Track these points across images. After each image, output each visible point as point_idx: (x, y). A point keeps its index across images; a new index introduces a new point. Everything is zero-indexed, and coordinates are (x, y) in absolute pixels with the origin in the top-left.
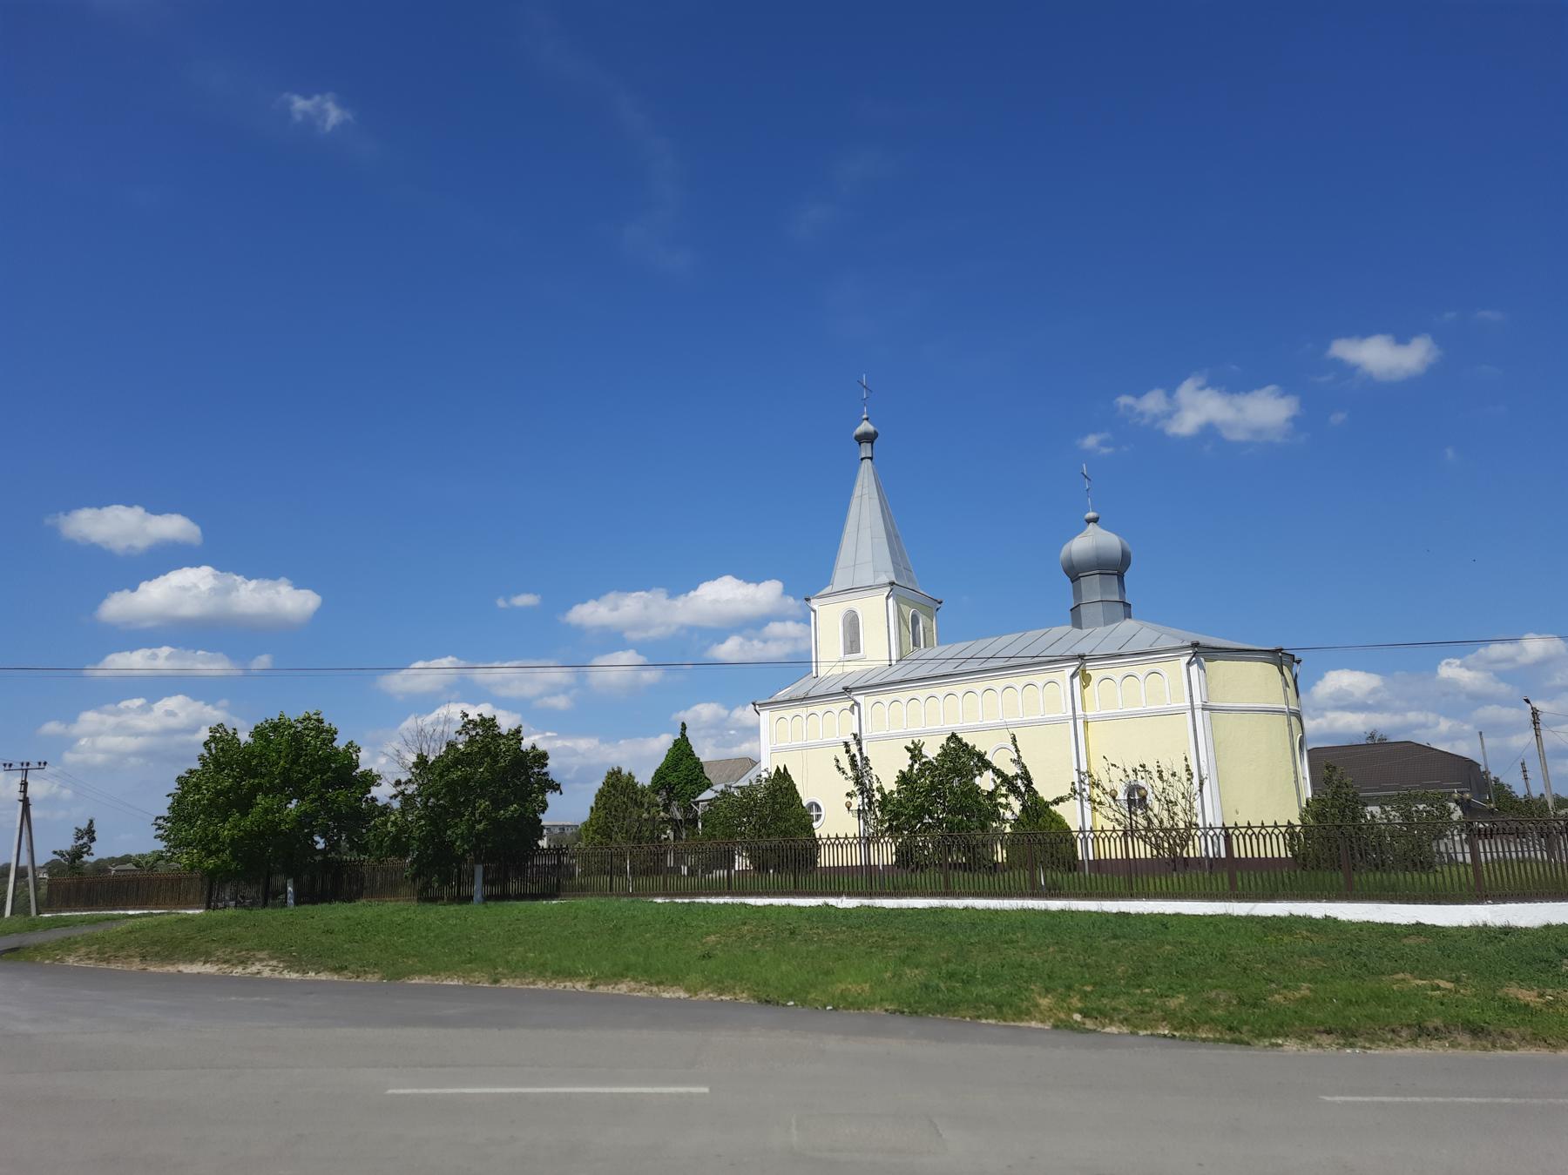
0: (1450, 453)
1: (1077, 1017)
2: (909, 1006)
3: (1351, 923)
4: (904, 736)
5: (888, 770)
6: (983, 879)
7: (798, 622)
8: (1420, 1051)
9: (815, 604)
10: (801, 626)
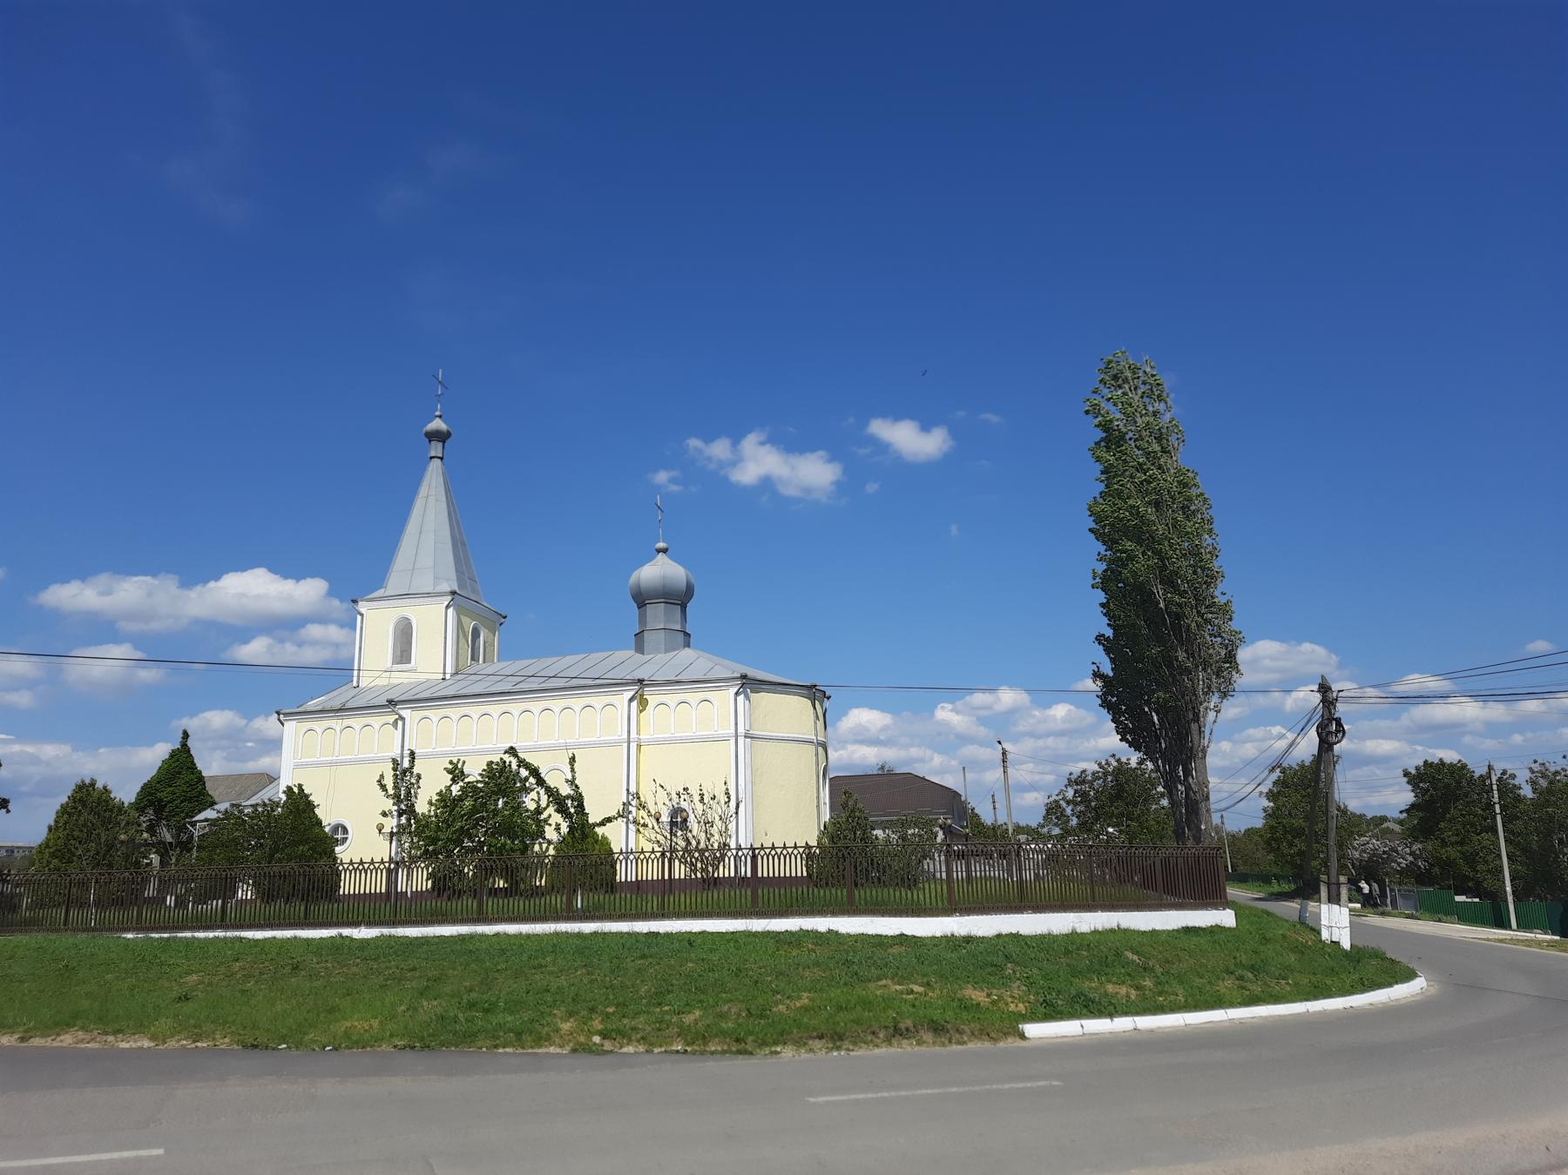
0: (954, 529)
1: (597, 1039)
2: (422, 1039)
3: (849, 935)
4: (444, 755)
5: (432, 785)
6: (519, 904)
7: (342, 626)
8: (892, 1050)
9: (363, 607)
10: (345, 631)
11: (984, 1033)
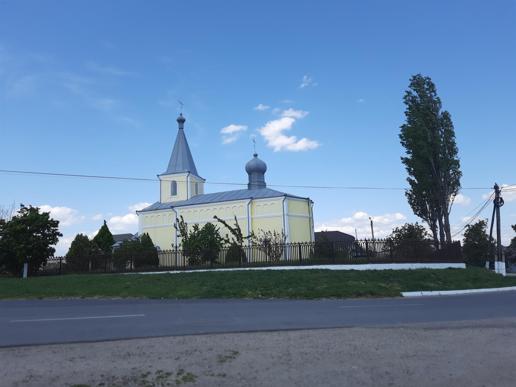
1: (260, 296)
5: (190, 230)
8: (359, 299)
11: (388, 295)
